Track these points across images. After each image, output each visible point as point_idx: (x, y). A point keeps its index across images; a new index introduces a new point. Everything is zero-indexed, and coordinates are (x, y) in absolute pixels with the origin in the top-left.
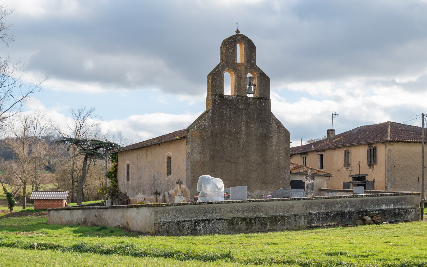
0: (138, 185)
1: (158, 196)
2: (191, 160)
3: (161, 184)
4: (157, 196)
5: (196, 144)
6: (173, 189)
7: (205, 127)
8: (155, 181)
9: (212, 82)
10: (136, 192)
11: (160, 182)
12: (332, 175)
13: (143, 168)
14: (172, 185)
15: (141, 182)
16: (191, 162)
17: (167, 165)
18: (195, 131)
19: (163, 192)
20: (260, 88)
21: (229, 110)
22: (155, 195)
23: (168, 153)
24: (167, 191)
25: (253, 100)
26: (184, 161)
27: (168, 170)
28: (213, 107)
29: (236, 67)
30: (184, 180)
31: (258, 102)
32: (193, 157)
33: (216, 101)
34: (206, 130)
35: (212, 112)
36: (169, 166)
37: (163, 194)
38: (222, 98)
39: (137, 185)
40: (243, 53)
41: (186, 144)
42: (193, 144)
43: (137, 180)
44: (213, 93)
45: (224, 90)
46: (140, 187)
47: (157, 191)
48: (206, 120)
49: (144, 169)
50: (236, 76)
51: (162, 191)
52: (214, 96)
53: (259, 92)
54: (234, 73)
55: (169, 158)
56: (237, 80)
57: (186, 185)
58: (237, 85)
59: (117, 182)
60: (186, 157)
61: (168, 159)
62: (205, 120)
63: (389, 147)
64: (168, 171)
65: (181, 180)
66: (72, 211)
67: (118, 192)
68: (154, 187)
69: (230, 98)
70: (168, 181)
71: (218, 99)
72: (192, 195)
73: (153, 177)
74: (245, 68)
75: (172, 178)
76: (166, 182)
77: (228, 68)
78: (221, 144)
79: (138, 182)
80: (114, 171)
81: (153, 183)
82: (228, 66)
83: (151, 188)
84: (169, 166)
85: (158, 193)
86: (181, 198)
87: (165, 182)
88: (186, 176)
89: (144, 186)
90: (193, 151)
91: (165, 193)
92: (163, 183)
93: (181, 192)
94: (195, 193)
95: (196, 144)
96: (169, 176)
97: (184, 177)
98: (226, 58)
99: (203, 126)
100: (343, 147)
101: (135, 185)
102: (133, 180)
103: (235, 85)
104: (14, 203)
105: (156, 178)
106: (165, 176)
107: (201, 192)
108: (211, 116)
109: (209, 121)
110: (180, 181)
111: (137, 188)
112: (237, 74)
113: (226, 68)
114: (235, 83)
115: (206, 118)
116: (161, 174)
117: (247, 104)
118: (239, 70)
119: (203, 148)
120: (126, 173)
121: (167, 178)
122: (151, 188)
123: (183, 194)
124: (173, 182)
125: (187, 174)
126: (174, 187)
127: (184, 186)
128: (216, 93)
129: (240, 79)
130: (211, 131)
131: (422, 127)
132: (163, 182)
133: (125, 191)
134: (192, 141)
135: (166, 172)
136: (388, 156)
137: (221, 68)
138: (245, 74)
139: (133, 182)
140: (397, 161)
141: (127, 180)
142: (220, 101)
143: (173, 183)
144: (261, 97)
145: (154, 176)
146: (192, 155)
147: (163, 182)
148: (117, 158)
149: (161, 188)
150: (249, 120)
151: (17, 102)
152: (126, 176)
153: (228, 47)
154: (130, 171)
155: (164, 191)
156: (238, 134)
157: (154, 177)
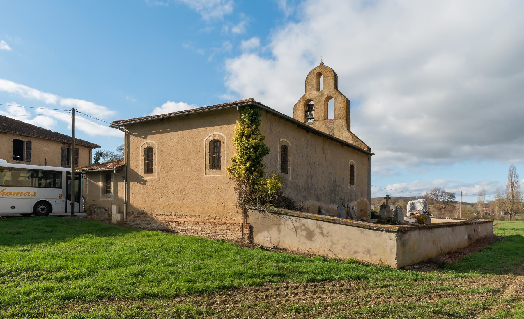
6: (356, 201)
11: (342, 190)
23: (281, 140)
36: (352, 175)
55: (352, 167)
57: (368, 199)
66: (454, 228)
68: (335, 194)
73: (333, 181)
81: (332, 188)
84: (352, 175)
100: (43, 139)
120: (279, 158)
121: (349, 187)
131: (72, 136)
145: (334, 181)
157: (334, 181)
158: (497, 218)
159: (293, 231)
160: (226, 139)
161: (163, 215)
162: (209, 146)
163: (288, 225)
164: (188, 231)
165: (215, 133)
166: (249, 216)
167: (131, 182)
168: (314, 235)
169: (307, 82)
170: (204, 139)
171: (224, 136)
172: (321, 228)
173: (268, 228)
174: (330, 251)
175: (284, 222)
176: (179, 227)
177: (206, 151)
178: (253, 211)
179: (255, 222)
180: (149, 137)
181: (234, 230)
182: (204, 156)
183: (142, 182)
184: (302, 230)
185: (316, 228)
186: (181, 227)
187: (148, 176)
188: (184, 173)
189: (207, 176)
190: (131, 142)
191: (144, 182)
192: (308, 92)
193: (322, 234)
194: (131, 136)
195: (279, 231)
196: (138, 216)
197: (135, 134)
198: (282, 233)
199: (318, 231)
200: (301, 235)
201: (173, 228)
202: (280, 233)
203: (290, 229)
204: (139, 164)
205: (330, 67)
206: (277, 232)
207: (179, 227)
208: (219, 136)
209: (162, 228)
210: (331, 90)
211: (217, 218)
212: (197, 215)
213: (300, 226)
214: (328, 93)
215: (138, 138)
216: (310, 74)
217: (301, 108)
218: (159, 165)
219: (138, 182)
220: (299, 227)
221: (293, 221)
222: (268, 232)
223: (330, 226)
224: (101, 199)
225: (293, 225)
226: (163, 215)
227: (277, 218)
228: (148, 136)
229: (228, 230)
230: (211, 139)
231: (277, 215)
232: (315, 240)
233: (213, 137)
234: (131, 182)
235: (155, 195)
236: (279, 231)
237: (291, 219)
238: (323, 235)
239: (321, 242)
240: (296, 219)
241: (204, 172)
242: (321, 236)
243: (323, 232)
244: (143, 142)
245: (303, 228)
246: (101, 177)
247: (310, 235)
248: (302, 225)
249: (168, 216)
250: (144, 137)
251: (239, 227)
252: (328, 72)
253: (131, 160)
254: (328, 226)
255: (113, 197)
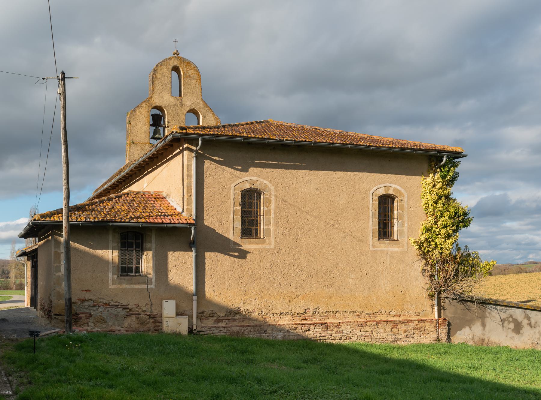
158: (13, 286)
159: (499, 324)
160: (406, 195)
161: (287, 313)
162: (377, 203)
163: (494, 317)
164: (346, 337)
165: (389, 185)
166: (445, 308)
167: (206, 253)
168: (522, 327)
169: (156, 77)
170: (369, 190)
171: (403, 191)
172: (529, 318)
173: (469, 323)
174: (538, 343)
175: (490, 313)
176: (330, 332)
177: (373, 210)
178: (451, 301)
179: (453, 316)
180: (252, 170)
181: (425, 330)
182: (371, 218)
183: (236, 254)
184: (509, 322)
185: (524, 318)
186: (333, 332)
187: (251, 243)
188: (332, 242)
189: (375, 249)
190: (206, 174)
191: (243, 254)
192: (157, 94)
193: (530, 324)
194: (207, 163)
195: (484, 325)
196: (225, 318)
197: (217, 158)
198: (487, 328)
199: (525, 322)
200: (509, 328)
201: (318, 335)
202: (484, 329)
203: (496, 321)
204: (229, 218)
205: (195, 64)
206: (481, 328)
207: (330, 332)
208: (395, 189)
209: (294, 337)
210: (197, 101)
211: (393, 313)
212: (357, 310)
213: (507, 318)
214: (192, 104)
215: (225, 167)
216: (161, 65)
217: (145, 119)
218: (278, 225)
219: (226, 253)
220: (506, 319)
221: (499, 312)
222: (470, 328)
223: (538, 315)
224: (112, 287)
225: (499, 316)
226: (287, 313)
227: (481, 309)
228: (251, 168)
229: (416, 330)
230: (382, 192)
231: (481, 305)
232: (523, 333)
233: (385, 190)
234: (206, 253)
235: (269, 278)
236: (484, 325)
237: (497, 309)
238: (531, 327)
239: (528, 335)
240: (503, 309)
241: (371, 243)
242: (529, 327)
243: (531, 323)
244: (239, 177)
245: (511, 319)
246: (112, 238)
247: (518, 328)
248: (509, 316)
249: (298, 314)
250: (240, 168)
251: (433, 325)
252: (192, 71)
253: (205, 209)
254: (536, 315)
255: (153, 283)
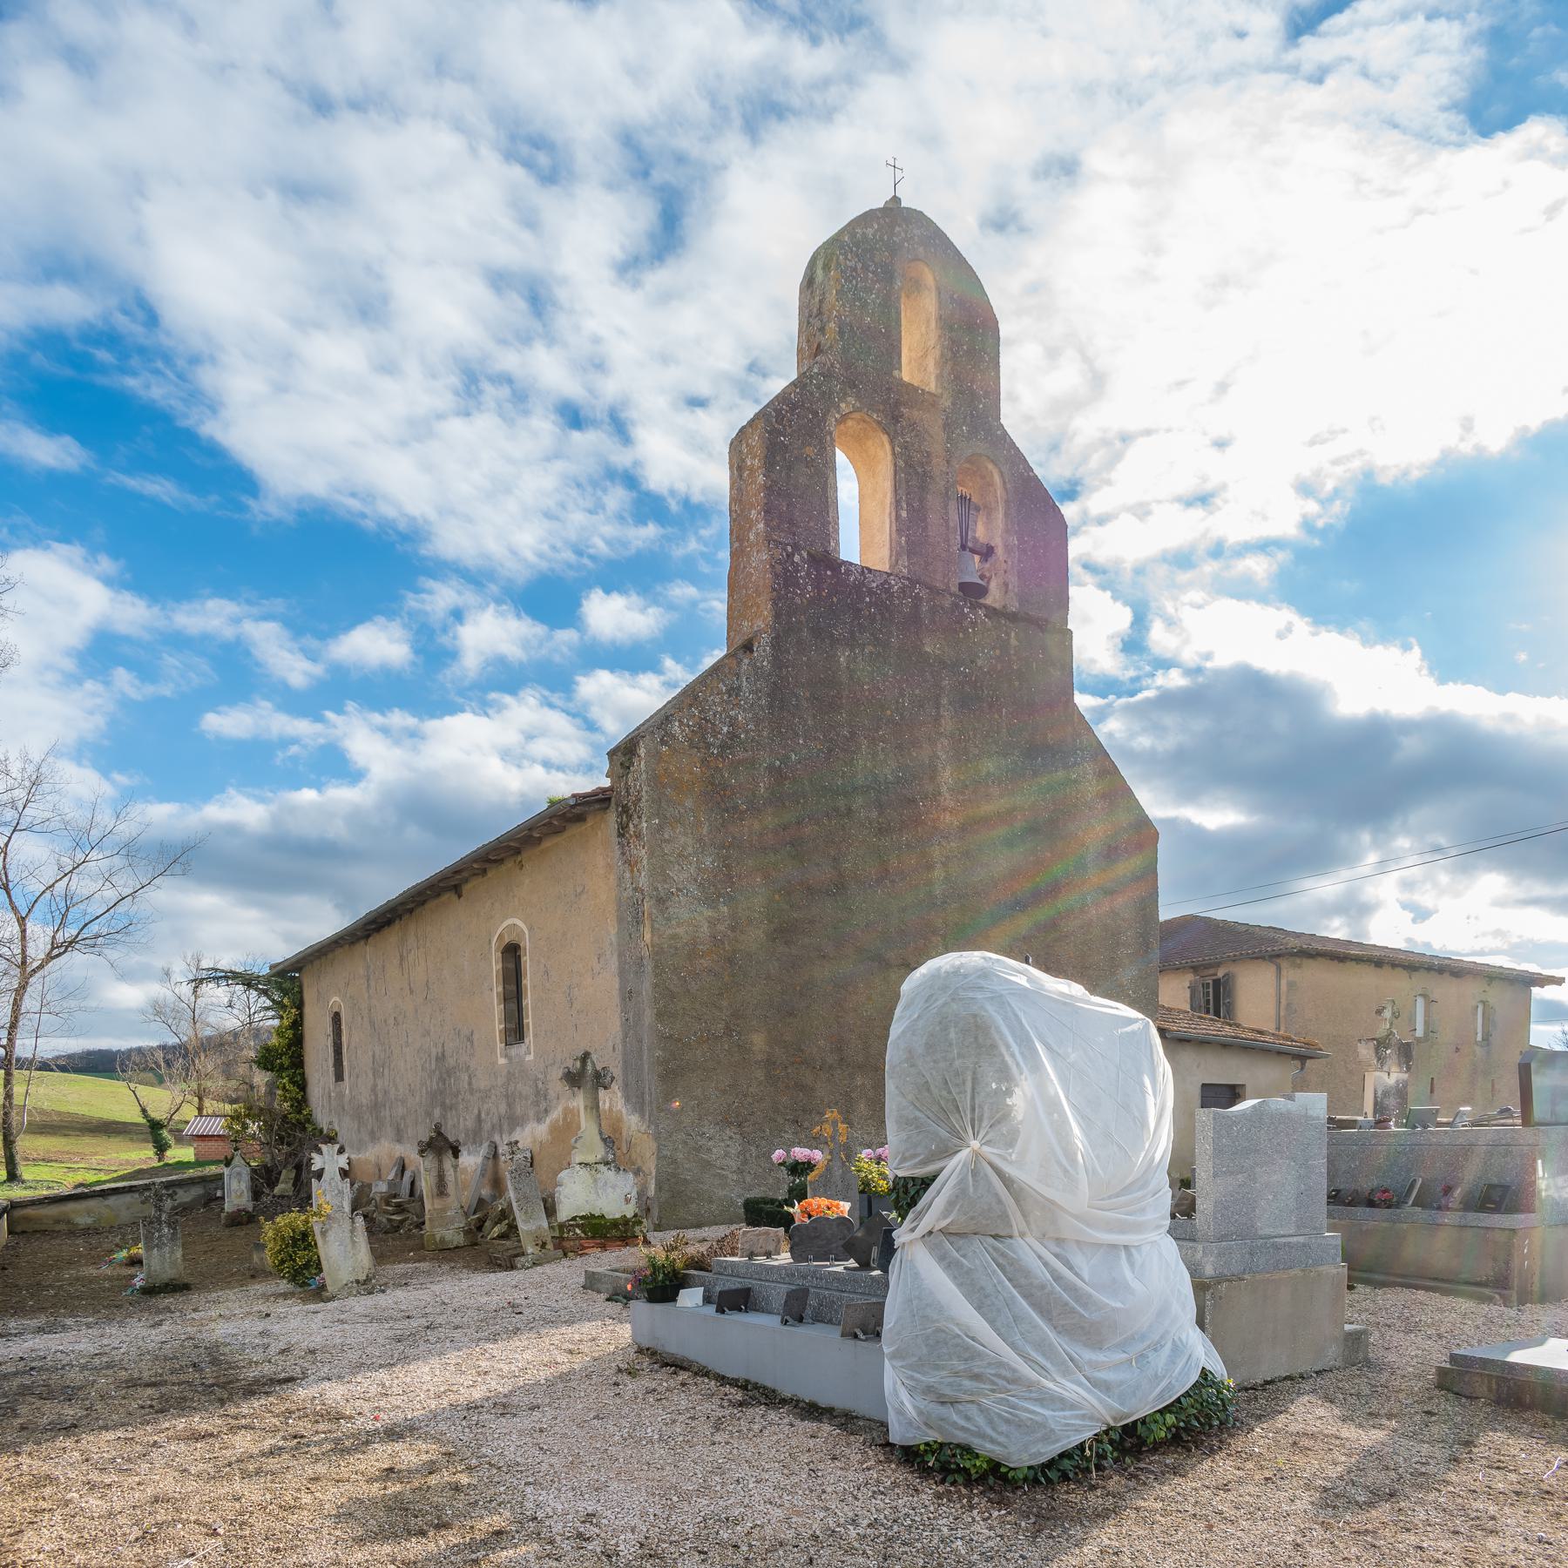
0: (376, 1096)
1: (448, 1162)
2: (653, 935)
3: (472, 1091)
4: (440, 1162)
5: (683, 840)
6: (539, 1120)
7: (733, 736)
8: (445, 1076)
9: (769, 464)
10: (369, 1127)
11: (470, 1084)
12: (1321, 1050)
13: (391, 1021)
14: (532, 1098)
15: (386, 1084)
16: (658, 952)
17: (500, 989)
18: (673, 750)
19: (485, 1135)
20: (1020, 561)
21: (871, 653)
22: (430, 1157)
24: (505, 1127)
25: (990, 618)
26: (608, 953)
27: (507, 1018)
28: (777, 616)
29: (898, 404)
30: (607, 1057)
31: (1013, 634)
32: (668, 919)
33: (797, 585)
34: (741, 755)
35: (773, 647)
37: (486, 1145)
38: (829, 573)
39: (373, 1097)
40: (932, 343)
41: (615, 839)
42: (666, 836)
43: (371, 1075)
44: (773, 529)
45: (837, 531)
46: (385, 1106)
47: (440, 1134)
48: (739, 688)
49: (396, 1022)
50: (902, 463)
51: (480, 1129)
52: (785, 550)
53: (1013, 580)
54: (885, 438)
55: (512, 952)
56: (904, 485)
57: (627, 1099)
58: (904, 514)
59: (302, 1086)
60: (620, 920)
61: (504, 960)
62: (734, 691)
63: (1290, 974)
64: (510, 1023)
65: (598, 1061)
67: (304, 1129)
68: (443, 1105)
69: (874, 585)
70: (510, 1076)
71: (808, 574)
72: (665, 1157)
74: (947, 426)
75: (531, 1057)
76: (500, 1081)
77: (858, 397)
78: (832, 853)
79: (375, 1086)
80: (289, 1046)
82: (855, 386)
83: (429, 1114)
85: (446, 1139)
86: (600, 1184)
87: (496, 1078)
88: (626, 1036)
89: (399, 1103)
90: (666, 878)
91: (497, 1138)
92: (482, 1088)
93: (604, 1140)
94: (686, 1143)
95: (686, 834)
96: (514, 1050)
97: (611, 1044)
98: (841, 333)
99: (725, 729)
101: (365, 1098)
102: (357, 1077)
103: (898, 517)
104: (166, 1143)
105: (451, 1062)
106: (493, 1051)
107: (954, 1165)
108: (769, 675)
109: (759, 698)
110: (589, 1067)
111: (371, 1114)
112: (905, 447)
113: (845, 394)
114: (897, 503)
115: (738, 676)
116: (470, 1039)
117: (961, 635)
118: (913, 425)
119: (728, 867)
121: (502, 1061)
122: (429, 1114)
123: (616, 1153)
124: (537, 1079)
125: (630, 1026)
126: (543, 1105)
127: (612, 1099)
128: (794, 534)
129: (923, 488)
130: (771, 768)
132: (482, 1082)
133: (331, 1123)
134: (658, 815)
135: (499, 1026)
136: (1288, 1005)
137: (818, 387)
138: (948, 462)
139: (358, 1087)
140: (1311, 1020)
141: (336, 1081)
142: (818, 585)
143: (540, 1085)
144: (1027, 614)
146: (661, 901)
147: (482, 1082)
148: (301, 992)
149: (476, 1111)
150: (971, 733)
151: (123, 899)
152: (331, 1061)
153: (855, 269)
154: (344, 1039)
155: (493, 1127)
156: (918, 805)
157: (441, 1058)
